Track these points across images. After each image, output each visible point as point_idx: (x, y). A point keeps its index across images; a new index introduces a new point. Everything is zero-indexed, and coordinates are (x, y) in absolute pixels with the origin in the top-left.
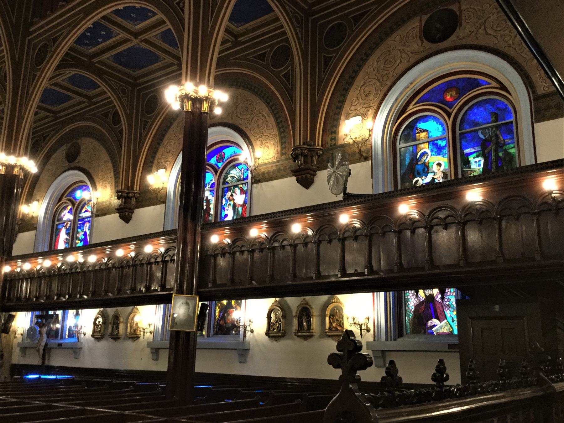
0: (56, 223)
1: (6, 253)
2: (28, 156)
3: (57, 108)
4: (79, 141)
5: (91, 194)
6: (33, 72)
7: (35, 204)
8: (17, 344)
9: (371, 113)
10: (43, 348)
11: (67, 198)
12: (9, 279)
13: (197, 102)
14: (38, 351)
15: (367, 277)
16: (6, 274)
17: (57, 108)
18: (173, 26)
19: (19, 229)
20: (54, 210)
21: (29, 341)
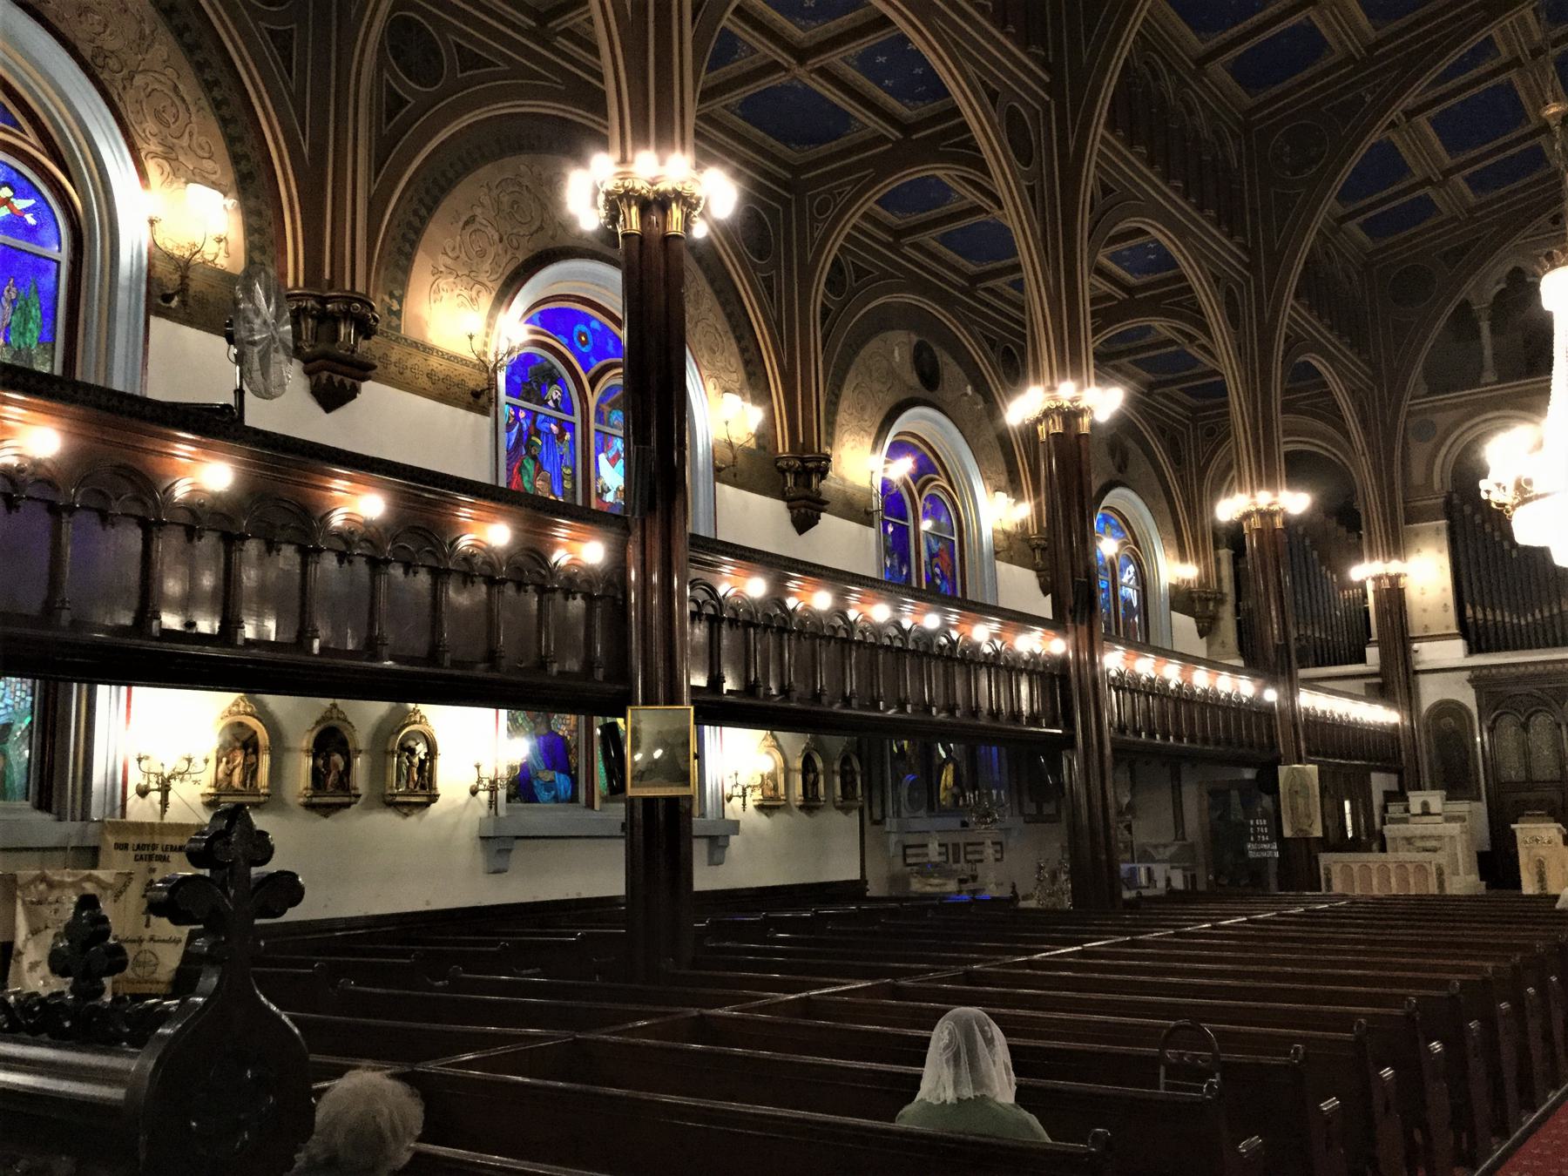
5: (885, 470)
9: (507, 300)
13: (654, 208)
15: (154, 643)
18: (725, 10)
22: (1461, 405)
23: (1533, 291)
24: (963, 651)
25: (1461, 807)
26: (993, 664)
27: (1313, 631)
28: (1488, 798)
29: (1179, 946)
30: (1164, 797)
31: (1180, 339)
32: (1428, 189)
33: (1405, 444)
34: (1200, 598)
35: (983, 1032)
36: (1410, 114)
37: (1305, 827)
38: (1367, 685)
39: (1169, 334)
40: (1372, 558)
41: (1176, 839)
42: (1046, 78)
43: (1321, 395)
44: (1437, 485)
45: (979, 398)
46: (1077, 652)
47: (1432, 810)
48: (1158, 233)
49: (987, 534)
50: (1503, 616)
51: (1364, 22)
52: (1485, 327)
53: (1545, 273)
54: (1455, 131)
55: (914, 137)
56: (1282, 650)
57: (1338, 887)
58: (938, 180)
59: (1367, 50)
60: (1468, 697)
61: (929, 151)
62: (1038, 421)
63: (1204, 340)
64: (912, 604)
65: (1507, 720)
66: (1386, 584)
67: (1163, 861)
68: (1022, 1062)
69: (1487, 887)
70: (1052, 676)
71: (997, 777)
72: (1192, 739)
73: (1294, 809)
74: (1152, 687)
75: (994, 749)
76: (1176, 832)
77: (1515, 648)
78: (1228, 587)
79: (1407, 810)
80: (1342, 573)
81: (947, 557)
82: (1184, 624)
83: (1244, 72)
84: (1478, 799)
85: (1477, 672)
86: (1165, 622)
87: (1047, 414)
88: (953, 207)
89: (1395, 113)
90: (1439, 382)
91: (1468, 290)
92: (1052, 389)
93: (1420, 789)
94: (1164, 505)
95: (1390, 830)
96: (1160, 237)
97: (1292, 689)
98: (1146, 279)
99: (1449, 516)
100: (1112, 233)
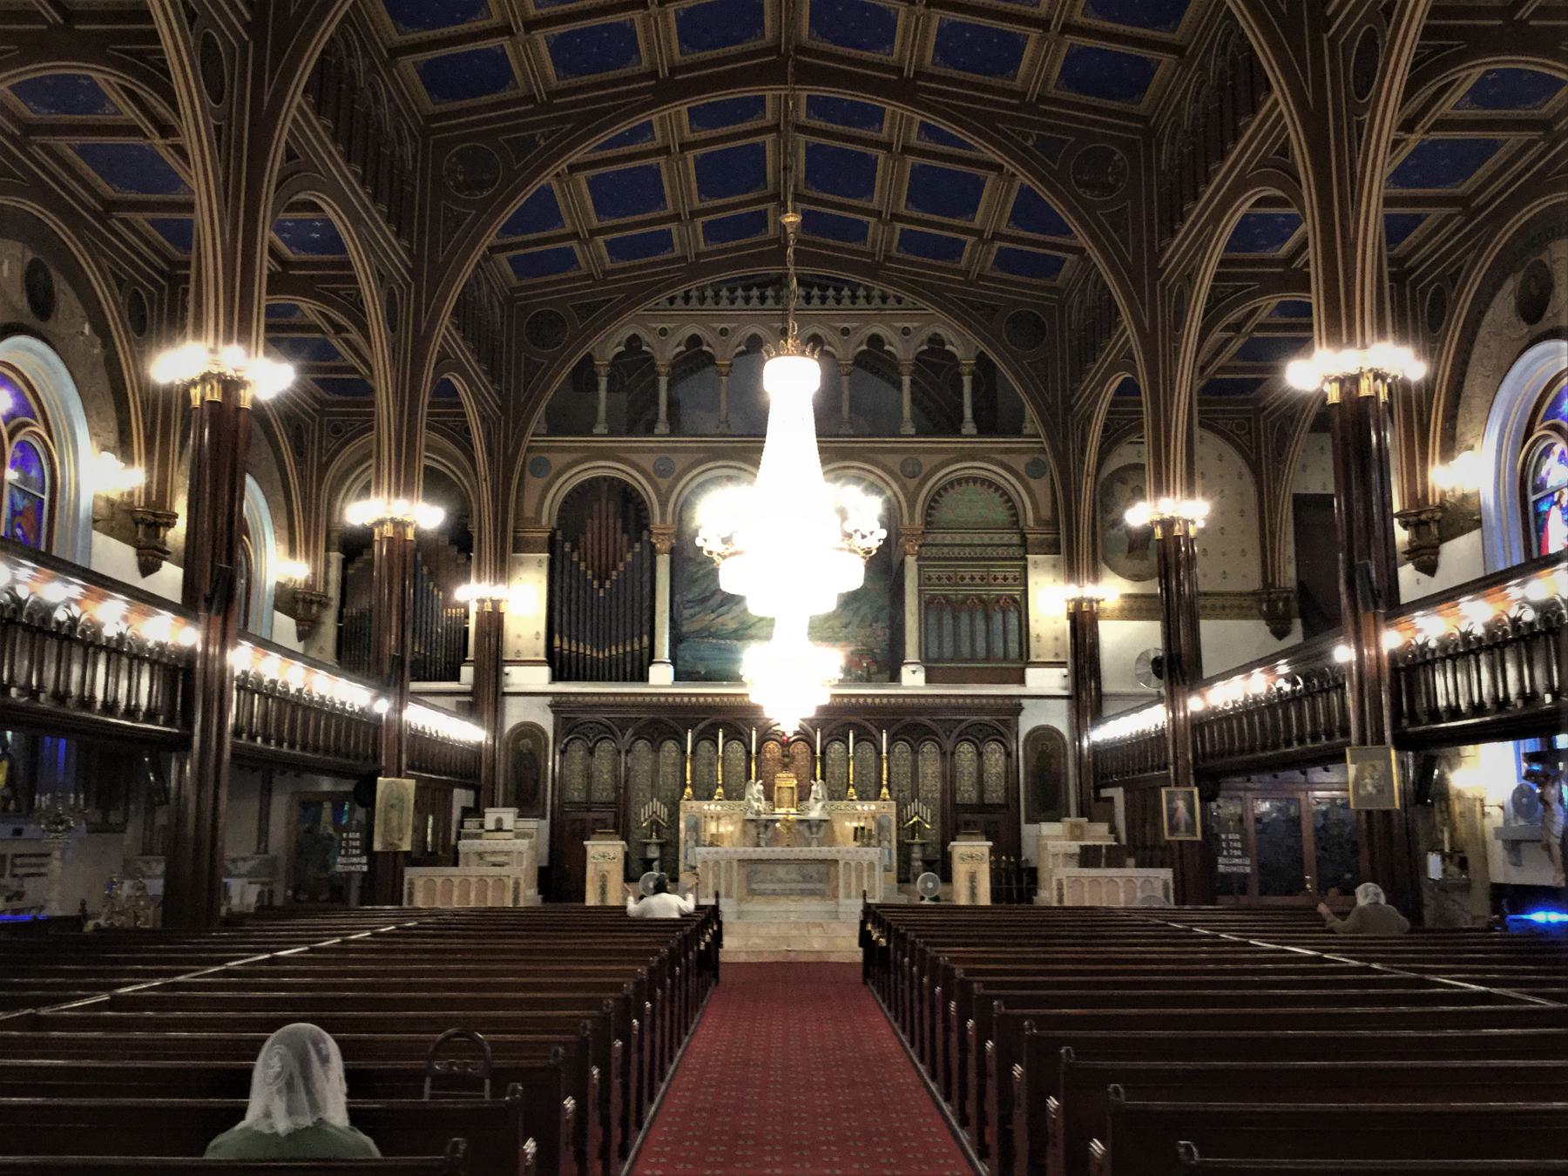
0: (1532, 498)
1: (1381, 602)
2: (1390, 335)
3: (1465, 187)
4: (1544, 257)
6: (1355, 118)
7: (1463, 459)
8: (1493, 832)
10: (1558, 841)
11: (1546, 424)
12: (1401, 665)
14: (1548, 848)
16: (1393, 656)
17: (1465, 187)
19: (1440, 533)
20: (1519, 466)
21: (1522, 822)
22: (576, 449)
23: (755, 375)
24: (83, 632)
25: (531, 824)
26: (115, 650)
27: (585, 649)
28: (552, 818)
29: (314, 961)
30: (253, 806)
31: (326, 326)
32: (574, 244)
33: (521, 478)
34: (304, 600)
35: (319, 1052)
36: (573, 168)
37: (396, 842)
38: (458, 703)
39: (313, 318)
40: (479, 579)
41: (258, 853)
42: (248, 17)
43: (458, 415)
44: (544, 521)
45: (98, 341)
46: (206, 643)
47: (505, 827)
48: (331, 211)
49: (86, 503)
50: (585, 649)
51: (550, 69)
52: (603, 383)
53: (770, 358)
54: (608, 195)
55: (77, 27)
56: (399, 663)
57: (420, 901)
58: (94, 85)
59: (548, 94)
60: (546, 721)
61: (94, 49)
62: (194, 383)
63: (355, 335)
64: (34, 569)
65: (578, 743)
66: (488, 607)
67: (240, 876)
68: (357, 1083)
69: (544, 900)
70: (175, 669)
71: (61, 778)
72: (304, 748)
73: (387, 822)
74: (274, 689)
75: (63, 742)
76: (259, 844)
77: (577, 679)
78: (334, 592)
79: (482, 826)
80: (448, 592)
81: (32, 518)
82: (285, 627)
83: (434, 77)
84: (543, 817)
85: (557, 699)
86: (266, 619)
87: (205, 378)
88: (106, 118)
89: (562, 165)
90: (559, 424)
91: (592, 345)
92: (214, 351)
93: (493, 806)
94: (281, 498)
95: (464, 845)
96: (335, 219)
97: (401, 703)
98: (304, 256)
99: (551, 552)
100: (295, 198)
